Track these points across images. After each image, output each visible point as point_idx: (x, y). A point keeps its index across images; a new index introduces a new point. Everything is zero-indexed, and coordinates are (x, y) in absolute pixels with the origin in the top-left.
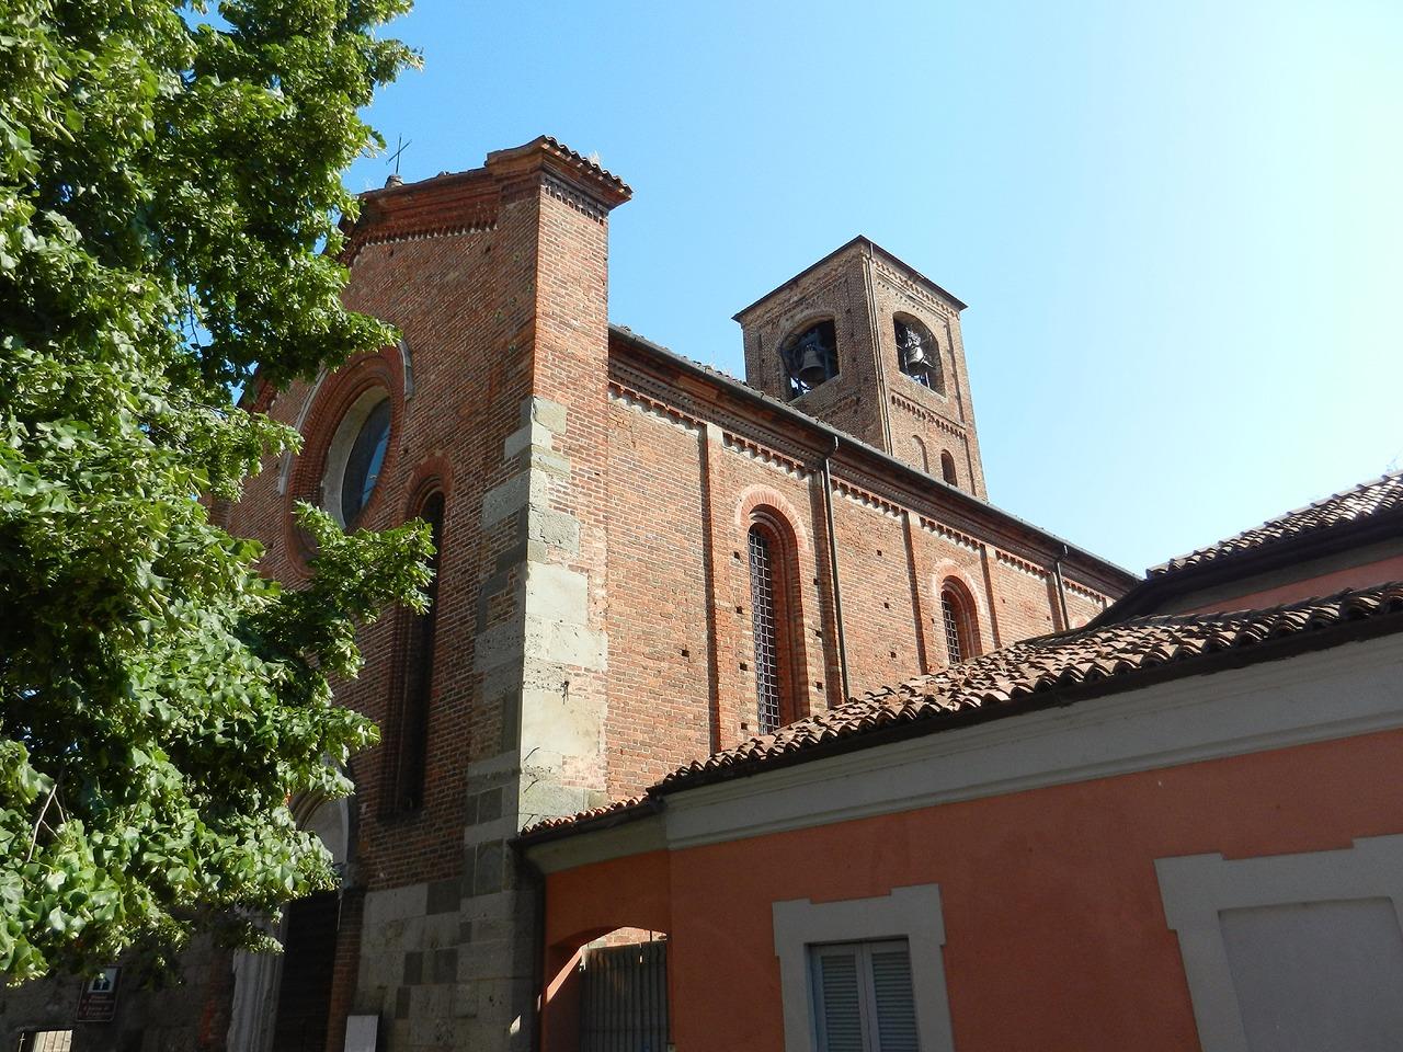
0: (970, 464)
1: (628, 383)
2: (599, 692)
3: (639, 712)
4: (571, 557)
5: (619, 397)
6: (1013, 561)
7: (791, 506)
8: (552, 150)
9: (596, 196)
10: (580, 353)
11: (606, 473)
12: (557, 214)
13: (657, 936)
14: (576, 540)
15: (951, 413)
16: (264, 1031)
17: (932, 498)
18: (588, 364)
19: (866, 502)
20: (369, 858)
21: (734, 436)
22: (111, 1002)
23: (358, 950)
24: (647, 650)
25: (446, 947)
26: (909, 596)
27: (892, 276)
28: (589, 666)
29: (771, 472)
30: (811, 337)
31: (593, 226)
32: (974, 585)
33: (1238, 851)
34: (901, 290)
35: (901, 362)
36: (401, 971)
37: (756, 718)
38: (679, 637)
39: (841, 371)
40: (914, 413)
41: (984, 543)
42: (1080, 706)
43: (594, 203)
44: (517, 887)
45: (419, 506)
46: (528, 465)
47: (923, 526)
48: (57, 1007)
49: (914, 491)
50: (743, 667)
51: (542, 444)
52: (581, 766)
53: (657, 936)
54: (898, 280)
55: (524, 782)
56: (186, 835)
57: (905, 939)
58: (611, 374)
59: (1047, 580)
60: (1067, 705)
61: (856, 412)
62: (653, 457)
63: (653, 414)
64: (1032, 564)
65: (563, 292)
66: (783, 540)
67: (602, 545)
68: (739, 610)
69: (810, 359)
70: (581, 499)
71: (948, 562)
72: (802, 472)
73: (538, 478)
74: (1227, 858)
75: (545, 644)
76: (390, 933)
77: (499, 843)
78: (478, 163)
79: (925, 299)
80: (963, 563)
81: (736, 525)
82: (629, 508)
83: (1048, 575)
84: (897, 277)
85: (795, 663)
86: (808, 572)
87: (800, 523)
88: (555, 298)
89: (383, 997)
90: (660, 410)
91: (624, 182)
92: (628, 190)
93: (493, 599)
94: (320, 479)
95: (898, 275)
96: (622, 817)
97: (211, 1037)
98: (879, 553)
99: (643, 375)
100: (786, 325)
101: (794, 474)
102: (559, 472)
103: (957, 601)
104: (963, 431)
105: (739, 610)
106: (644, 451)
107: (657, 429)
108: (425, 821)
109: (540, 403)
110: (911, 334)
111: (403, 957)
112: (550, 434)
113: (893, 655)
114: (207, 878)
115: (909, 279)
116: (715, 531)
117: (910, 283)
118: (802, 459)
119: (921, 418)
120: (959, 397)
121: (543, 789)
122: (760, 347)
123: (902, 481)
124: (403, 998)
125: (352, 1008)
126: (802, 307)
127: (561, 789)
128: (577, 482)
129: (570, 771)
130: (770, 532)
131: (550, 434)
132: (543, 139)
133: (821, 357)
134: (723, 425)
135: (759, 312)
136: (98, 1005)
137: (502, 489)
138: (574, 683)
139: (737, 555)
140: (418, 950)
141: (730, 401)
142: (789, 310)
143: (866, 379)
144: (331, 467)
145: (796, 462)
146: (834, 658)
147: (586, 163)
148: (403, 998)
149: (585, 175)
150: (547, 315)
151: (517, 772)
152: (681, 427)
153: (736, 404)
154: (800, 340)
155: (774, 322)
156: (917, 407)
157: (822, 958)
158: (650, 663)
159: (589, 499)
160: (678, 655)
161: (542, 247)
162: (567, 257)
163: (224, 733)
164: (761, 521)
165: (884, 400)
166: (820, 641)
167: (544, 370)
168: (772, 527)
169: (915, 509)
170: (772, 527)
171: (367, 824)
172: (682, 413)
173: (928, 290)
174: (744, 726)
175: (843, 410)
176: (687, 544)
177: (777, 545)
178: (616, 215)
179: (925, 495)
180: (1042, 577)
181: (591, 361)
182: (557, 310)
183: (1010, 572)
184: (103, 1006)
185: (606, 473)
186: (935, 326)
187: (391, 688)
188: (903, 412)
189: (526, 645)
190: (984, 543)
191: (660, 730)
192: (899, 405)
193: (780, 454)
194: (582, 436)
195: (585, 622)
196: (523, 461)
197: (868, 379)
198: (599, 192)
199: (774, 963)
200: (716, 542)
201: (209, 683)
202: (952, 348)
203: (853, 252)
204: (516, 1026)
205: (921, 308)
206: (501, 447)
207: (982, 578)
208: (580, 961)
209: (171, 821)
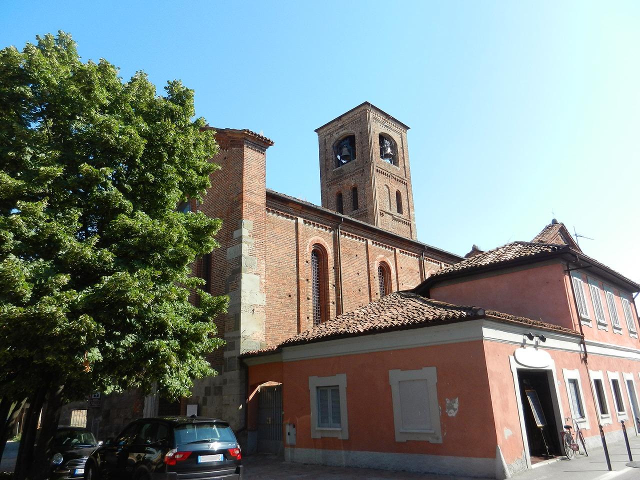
1: (272, 207)
3: (275, 315)
4: (255, 271)
10: (257, 202)
13: (279, 384)
14: (256, 265)
15: (401, 174)
16: (155, 410)
18: (260, 206)
19: (353, 238)
24: (278, 296)
25: (218, 386)
26: (366, 269)
27: (379, 117)
29: (319, 232)
30: (346, 142)
31: (261, 156)
32: (391, 263)
33: (404, 368)
35: (381, 153)
36: (204, 392)
37: (312, 315)
38: (288, 291)
44: (240, 370)
46: (241, 242)
47: (373, 244)
49: (370, 232)
50: (308, 299)
51: (245, 235)
52: (258, 334)
53: (279, 384)
55: (242, 340)
57: (338, 386)
58: (267, 205)
61: (362, 175)
63: (280, 216)
65: (251, 182)
67: (264, 265)
68: (307, 280)
69: (345, 151)
71: (381, 256)
73: (245, 246)
75: (247, 298)
77: (235, 357)
79: (393, 126)
80: (387, 256)
83: (419, 257)
84: (381, 118)
86: (331, 264)
87: (329, 248)
92: (272, 143)
93: (231, 283)
96: (270, 353)
97: (138, 411)
98: (357, 256)
100: (336, 136)
101: (328, 231)
102: (250, 243)
103: (384, 269)
104: (405, 182)
105: (307, 280)
109: (245, 221)
110: (386, 141)
113: (360, 290)
115: (386, 118)
116: (300, 255)
117: (386, 120)
120: (405, 167)
122: (325, 144)
124: (205, 400)
129: (255, 336)
130: (319, 252)
133: (349, 151)
134: (303, 218)
137: (233, 248)
138: (256, 310)
139: (307, 262)
140: (209, 386)
145: (328, 227)
147: (259, 136)
148: (205, 400)
149: (258, 140)
151: (240, 337)
152: (289, 220)
154: (341, 143)
155: (331, 134)
156: (387, 173)
158: (279, 300)
161: (245, 167)
162: (253, 169)
165: (373, 171)
167: (246, 209)
173: (394, 122)
174: (308, 318)
176: (291, 260)
179: (374, 233)
180: (417, 258)
181: (260, 204)
182: (250, 188)
186: (396, 138)
188: (381, 175)
189: (242, 299)
194: (258, 230)
196: (240, 240)
197: (367, 162)
198: (262, 144)
199: (309, 391)
200: (300, 258)
202: (403, 146)
203: (363, 108)
204: (241, 407)
207: (394, 261)
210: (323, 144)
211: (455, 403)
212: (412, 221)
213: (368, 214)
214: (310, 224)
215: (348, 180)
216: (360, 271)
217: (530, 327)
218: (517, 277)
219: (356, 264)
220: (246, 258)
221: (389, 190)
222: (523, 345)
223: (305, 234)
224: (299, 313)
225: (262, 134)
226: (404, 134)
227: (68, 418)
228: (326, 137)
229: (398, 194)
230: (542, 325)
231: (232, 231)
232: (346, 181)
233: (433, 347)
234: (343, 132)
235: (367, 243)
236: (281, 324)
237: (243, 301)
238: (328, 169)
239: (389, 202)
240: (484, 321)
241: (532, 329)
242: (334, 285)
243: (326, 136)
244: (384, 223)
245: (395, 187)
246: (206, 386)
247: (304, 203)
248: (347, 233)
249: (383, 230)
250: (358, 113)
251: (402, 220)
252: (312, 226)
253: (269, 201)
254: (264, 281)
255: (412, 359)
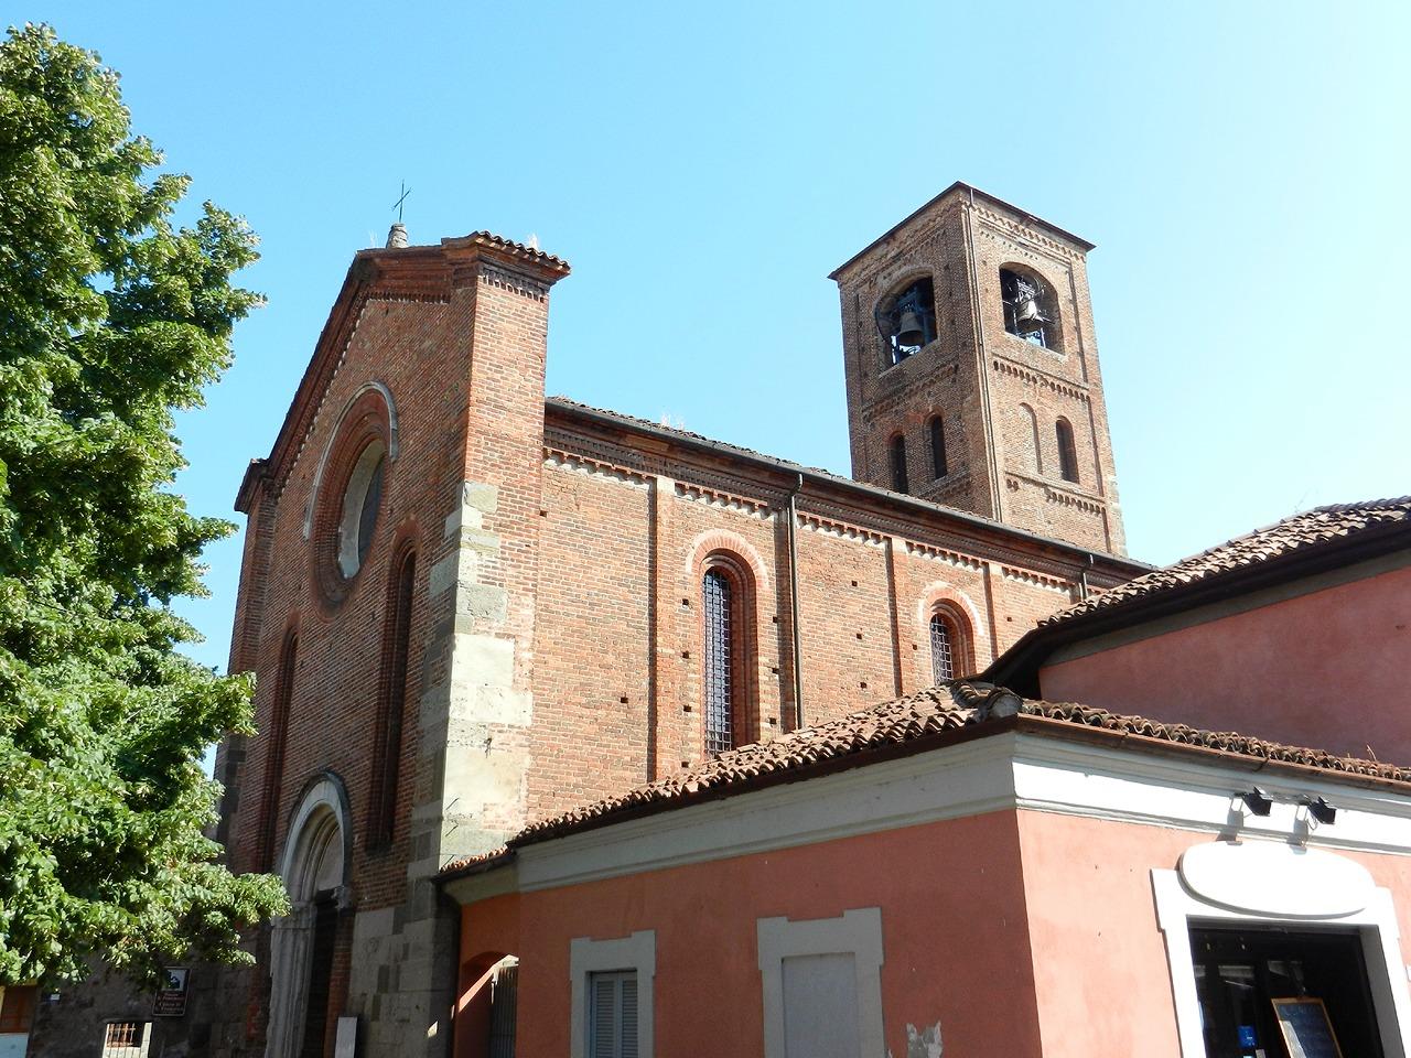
0: (1093, 429)
2: (521, 746)
3: (573, 757)
4: (499, 625)
5: (563, 463)
6: (1026, 576)
7: (751, 548)
8: (486, 243)
9: (534, 276)
10: (514, 433)
11: (536, 544)
12: (495, 300)
14: (503, 609)
16: (296, 1028)
17: (922, 521)
18: (522, 442)
20: (358, 883)
21: (687, 485)
22: (181, 999)
23: (349, 962)
24: (584, 700)
26: (888, 624)
28: (512, 723)
29: (729, 515)
30: (910, 296)
31: (533, 306)
34: (1010, 237)
38: (619, 686)
39: (939, 335)
40: (1023, 377)
41: (987, 561)
42: (731, 801)
43: (535, 282)
44: (437, 916)
45: (401, 564)
46: (458, 546)
48: (136, 1003)
50: (687, 709)
52: (501, 811)
54: (1007, 226)
55: (445, 828)
56: (53, 902)
59: (1072, 592)
60: (723, 799)
61: (954, 381)
62: (598, 517)
63: (599, 475)
64: (1049, 577)
66: (742, 580)
68: (686, 655)
69: (909, 322)
70: (511, 571)
71: (940, 585)
72: (766, 511)
74: (795, 917)
75: (469, 706)
76: (370, 949)
78: (434, 241)
80: (961, 584)
81: (687, 571)
82: (571, 569)
83: (1071, 586)
84: (1005, 223)
85: (749, 700)
88: (490, 384)
89: (364, 1003)
90: (607, 470)
91: (561, 260)
94: (339, 524)
95: (1006, 220)
98: (854, 584)
99: (588, 439)
100: (884, 284)
102: (490, 549)
105: (686, 655)
106: (589, 513)
107: (604, 489)
108: (393, 854)
109: (471, 486)
110: (1022, 286)
111: (377, 969)
112: (480, 514)
113: (863, 685)
114: (68, 925)
115: (1021, 223)
117: (1021, 227)
118: (765, 499)
119: (1031, 383)
120: (1081, 353)
121: (464, 833)
122: (858, 308)
123: (885, 508)
124: (377, 1002)
125: (344, 1012)
126: (899, 263)
127: (481, 833)
128: (507, 556)
129: (490, 816)
130: (728, 574)
131: (480, 514)
132: (476, 235)
133: (919, 319)
134: (675, 476)
135: (856, 269)
136: (170, 1002)
141: (682, 452)
142: (887, 267)
143: (964, 344)
144: (347, 513)
145: (757, 503)
146: (790, 694)
147: (521, 248)
148: (377, 1002)
149: (522, 260)
150: (481, 402)
151: (440, 819)
152: (630, 483)
153: (689, 454)
155: (871, 281)
156: (1026, 370)
157: (624, 982)
158: (586, 712)
159: (518, 570)
160: (616, 702)
163: (90, 836)
164: (719, 564)
166: (777, 677)
167: (476, 453)
168: (731, 568)
169: (902, 534)
170: (731, 568)
171: (357, 853)
172: (629, 470)
173: (1044, 232)
175: (942, 379)
176: (631, 597)
177: (738, 585)
178: (558, 289)
179: (913, 519)
181: (526, 439)
182: (492, 395)
183: (1020, 589)
184: (175, 1002)
185: (536, 544)
186: (1054, 274)
187: (377, 732)
190: (987, 561)
191: (595, 773)
192: (1003, 371)
193: (740, 497)
194: (513, 512)
195: (511, 684)
197: (966, 345)
198: (536, 272)
201: (50, 818)
203: (951, 200)
205: (1035, 255)
206: (443, 525)
208: (492, 977)
209: (44, 894)
210: (851, 310)
211: (933, 1042)
212: (1109, 502)
213: (971, 487)
214: (698, 496)
215: (918, 398)
216: (867, 629)
217: (1260, 768)
218: (1302, 611)
219: (854, 608)
220: (471, 590)
221: (1034, 416)
222: (1230, 832)
223: (678, 523)
224: (652, 750)
225: (533, 243)
226: (1077, 264)
227: (95, 1044)
228: (859, 291)
229: (1064, 429)
230: (1325, 763)
231: (443, 517)
232: (911, 402)
233: (873, 836)
234: (900, 272)
235: (889, 546)
236: (593, 782)
237: (454, 712)
238: (866, 375)
239: (1034, 450)
240: (1018, 737)
241: (1266, 773)
242: (775, 671)
243: (858, 286)
244: (1016, 511)
245: (1052, 409)
246: (382, 963)
247: (673, 435)
248: (820, 519)
249: (1035, 536)
250: (937, 216)
251: (1077, 498)
252: (703, 500)
253: (553, 429)
254: (528, 655)
255: (815, 881)
